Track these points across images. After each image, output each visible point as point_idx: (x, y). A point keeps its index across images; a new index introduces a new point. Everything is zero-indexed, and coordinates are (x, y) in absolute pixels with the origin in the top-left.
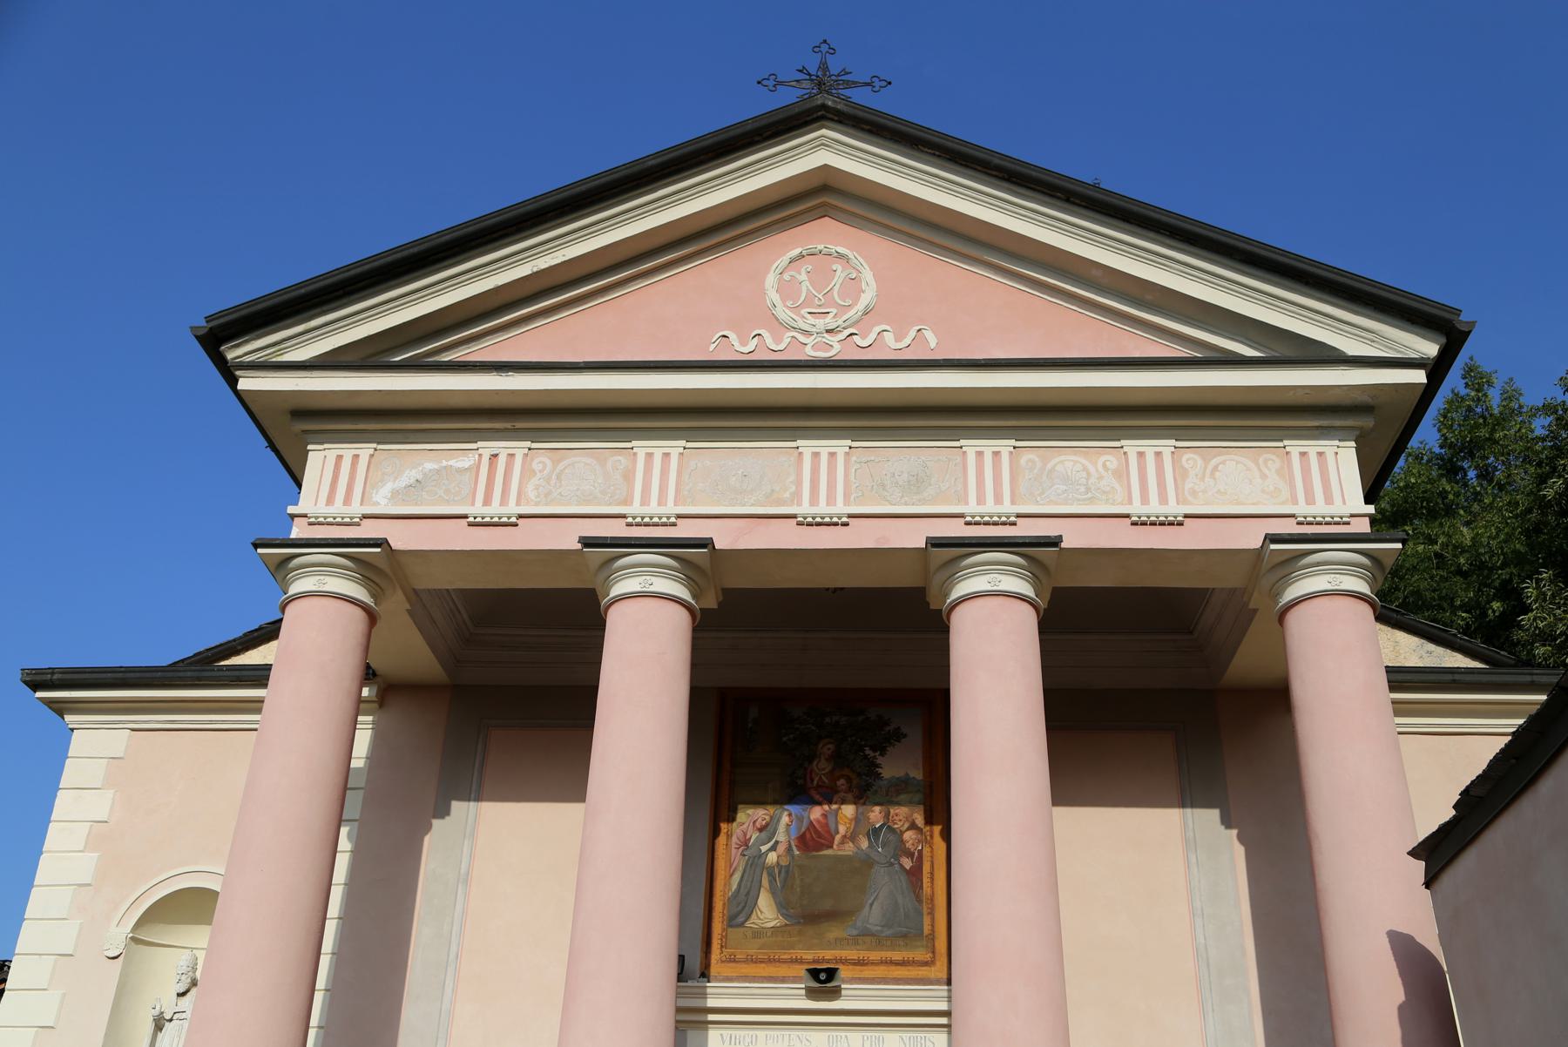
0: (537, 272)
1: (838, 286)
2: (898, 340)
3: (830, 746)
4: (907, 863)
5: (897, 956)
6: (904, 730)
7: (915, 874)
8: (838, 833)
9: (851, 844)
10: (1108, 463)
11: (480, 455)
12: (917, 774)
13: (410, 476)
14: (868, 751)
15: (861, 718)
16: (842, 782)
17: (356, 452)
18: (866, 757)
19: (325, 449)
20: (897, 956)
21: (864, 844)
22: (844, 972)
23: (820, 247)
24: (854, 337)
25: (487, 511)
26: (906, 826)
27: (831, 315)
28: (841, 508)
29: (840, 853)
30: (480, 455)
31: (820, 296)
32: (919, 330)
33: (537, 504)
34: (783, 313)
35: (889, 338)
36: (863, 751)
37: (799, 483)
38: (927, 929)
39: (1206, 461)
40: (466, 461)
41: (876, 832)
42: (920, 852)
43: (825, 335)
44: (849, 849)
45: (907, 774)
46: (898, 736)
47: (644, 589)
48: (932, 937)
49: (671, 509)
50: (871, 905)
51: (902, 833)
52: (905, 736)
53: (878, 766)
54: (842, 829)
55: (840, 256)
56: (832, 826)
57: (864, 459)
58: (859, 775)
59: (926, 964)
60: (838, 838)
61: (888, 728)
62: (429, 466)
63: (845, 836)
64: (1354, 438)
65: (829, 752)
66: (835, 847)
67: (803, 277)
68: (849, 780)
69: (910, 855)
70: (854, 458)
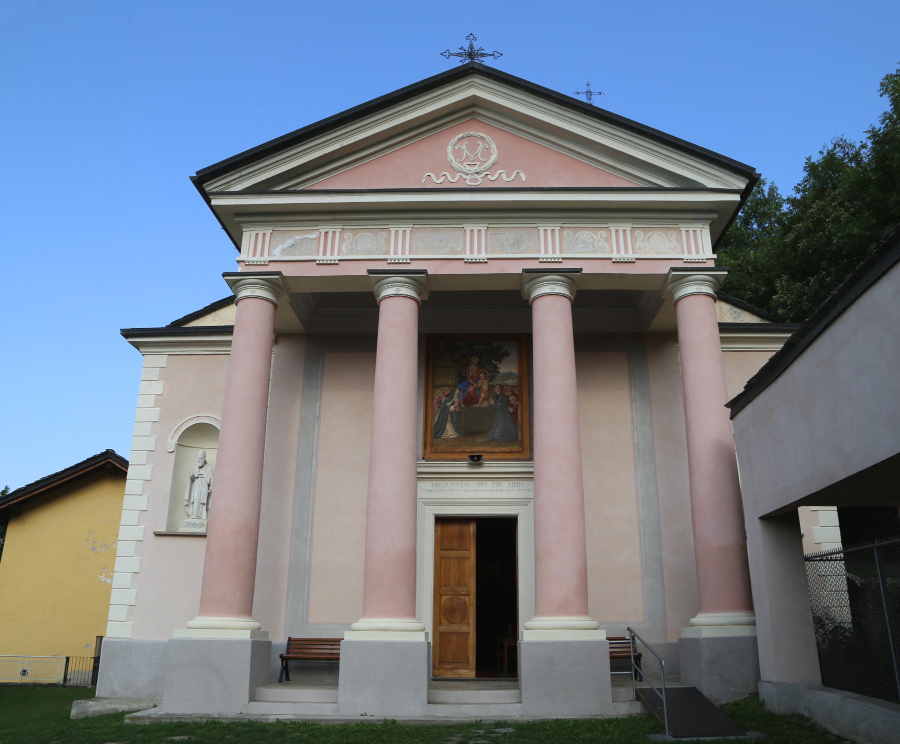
0: (343, 147)
1: (480, 153)
2: (508, 177)
3: (477, 359)
4: (511, 410)
5: (507, 449)
6: (509, 352)
7: (514, 415)
8: (480, 397)
9: (486, 402)
10: (602, 235)
11: (320, 232)
12: (515, 371)
13: (289, 242)
14: (493, 361)
16: (482, 375)
17: (264, 232)
18: (492, 364)
19: (250, 231)
20: (507, 449)
21: (492, 402)
22: (485, 456)
23: (472, 133)
24: (488, 176)
25: (325, 258)
26: (511, 394)
27: (477, 165)
28: (484, 255)
29: (482, 406)
30: (320, 232)
31: (472, 156)
32: (518, 173)
33: (347, 254)
34: (456, 164)
35: (504, 176)
36: (491, 361)
37: (465, 244)
38: (520, 438)
39: (354, 235)
40: (314, 236)
41: (498, 397)
42: (517, 405)
43: (475, 175)
44: (485, 404)
45: (511, 371)
46: (506, 354)
47: (397, 293)
48: (522, 441)
49: (408, 256)
50: (496, 427)
51: (509, 397)
52: (509, 354)
53: (498, 368)
54: (482, 396)
55: (481, 138)
56: (478, 394)
57: (494, 233)
58: (490, 372)
59: (519, 452)
60: (481, 399)
61: (502, 351)
62: (297, 237)
63: (483, 399)
64: (709, 224)
66: (479, 403)
67: (464, 147)
68: (485, 374)
69: (512, 406)
70: (489, 232)
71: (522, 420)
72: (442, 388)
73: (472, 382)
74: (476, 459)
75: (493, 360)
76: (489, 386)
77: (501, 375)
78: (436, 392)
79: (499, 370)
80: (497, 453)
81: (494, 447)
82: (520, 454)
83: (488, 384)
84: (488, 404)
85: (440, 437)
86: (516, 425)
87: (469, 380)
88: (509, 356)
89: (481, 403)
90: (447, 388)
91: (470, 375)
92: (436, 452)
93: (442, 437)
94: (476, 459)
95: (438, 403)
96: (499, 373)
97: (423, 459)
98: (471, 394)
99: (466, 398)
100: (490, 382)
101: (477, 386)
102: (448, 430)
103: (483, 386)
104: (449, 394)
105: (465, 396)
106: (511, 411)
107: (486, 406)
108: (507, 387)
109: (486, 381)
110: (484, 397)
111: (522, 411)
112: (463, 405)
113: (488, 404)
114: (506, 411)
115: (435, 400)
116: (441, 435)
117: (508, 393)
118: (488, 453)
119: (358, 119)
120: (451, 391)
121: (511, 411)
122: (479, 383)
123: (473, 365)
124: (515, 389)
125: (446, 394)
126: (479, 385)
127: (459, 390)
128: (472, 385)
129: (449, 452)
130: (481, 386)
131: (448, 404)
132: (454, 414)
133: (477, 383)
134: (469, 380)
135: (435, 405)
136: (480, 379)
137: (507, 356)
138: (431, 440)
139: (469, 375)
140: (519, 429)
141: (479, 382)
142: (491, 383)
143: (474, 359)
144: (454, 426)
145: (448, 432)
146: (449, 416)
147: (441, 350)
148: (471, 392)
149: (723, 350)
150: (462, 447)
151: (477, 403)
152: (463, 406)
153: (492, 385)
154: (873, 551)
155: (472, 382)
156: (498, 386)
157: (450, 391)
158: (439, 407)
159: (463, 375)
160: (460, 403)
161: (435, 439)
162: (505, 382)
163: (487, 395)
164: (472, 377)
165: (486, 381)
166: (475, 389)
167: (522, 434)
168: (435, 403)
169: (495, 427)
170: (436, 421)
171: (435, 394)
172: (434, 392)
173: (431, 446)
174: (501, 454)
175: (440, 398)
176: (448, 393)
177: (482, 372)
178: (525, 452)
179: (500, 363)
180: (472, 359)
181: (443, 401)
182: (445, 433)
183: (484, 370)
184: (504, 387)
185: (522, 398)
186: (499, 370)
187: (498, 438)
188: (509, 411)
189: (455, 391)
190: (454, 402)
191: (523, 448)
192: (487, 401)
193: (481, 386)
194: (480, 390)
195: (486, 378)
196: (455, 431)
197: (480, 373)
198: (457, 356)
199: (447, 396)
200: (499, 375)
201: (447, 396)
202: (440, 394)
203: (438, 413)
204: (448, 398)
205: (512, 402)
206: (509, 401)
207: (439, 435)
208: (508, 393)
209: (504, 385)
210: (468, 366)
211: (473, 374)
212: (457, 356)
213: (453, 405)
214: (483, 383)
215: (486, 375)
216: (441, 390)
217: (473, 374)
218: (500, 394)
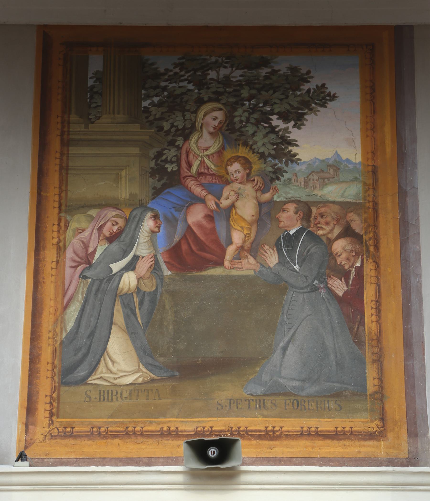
6: (331, 89)
8: (230, 242)
9: (251, 260)
14: (276, 121)
15: (264, 71)
18: (272, 130)
26: (337, 231)
29: (234, 272)
36: (268, 120)
42: (360, 270)
52: (333, 97)
53: (291, 143)
56: (222, 234)
58: (262, 156)
60: (231, 251)
61: (306, 87)
63: (241, 248)
65: (216, 123)
71: (379, 322)
72: (93, 212)
73: (198, 191)
74: (213, 453)
75: (275, 117)
76: (260, 204)
77: (304, 167)
78: (73, 225)
79: (294, 149)
80: (289, 436)
81: (280, 416)
82: (375, 443)
83: (257, 198)
84: (258, 268)
85: (83, 381)
86: (360, 343)
87: (191, 184)
88: (330, 104)
89: (231, 262)
90: (111, 213)
91: (194, 169)
92: (72, 435)
93: (92, 380)
94: (213, 453)
95: (80, 264)
96: (297, 162)
97: (22, 457)
98: (195, 229)
99: (178, 245)
100: (264, 192)
101: (217, 205)
102: (116, 357)
103: (238, 204)
104: (120, 232)
105: (177, 239)
106: (340, 293)
107: (251, 273)
108: (323, 210)
109: (248, 189)
110: (244, 242)
111: (378, 292)
112: (169, 269)
113: (258, 268)
114: (323, 292)
115: (69, 254)
116: (90, 374)
117: (328, 228)
118: (260, 437)
119: (242, 276)
120: (127, 221)
121: (340, 293)
122: (225, 194)
123: (205, 131)
124: (352, 216)
125: (106, 232)
126: (225, 203)
127: (156, 217)
128: (202, 201)
129: (115, 436)
130: (233, 206)
131: (116, 267)
132: (136, 300)
133: (219, 197)
134: (191, 184)
135: (68, 271)
136: (228, 183)
137: (324, 105)
138: (54, 389)
139: (190, 165)
140: (369, 356)
141: (226, 191)
142: (267, 196)
143: (214, 110)
144: (134, 342)
145: (113, 362)
146: (118, 307)
147: (90, 83)
148: (200, 226)
149: (110, 392)
150: (164, 416)
151: (220, 263)
152: (167, 272)
153: (271, 202)
154: (133, 296)
155: (198, 191)
156: (291, 207)
157: (121, 222)
158: (84, 277)
159: (170, 168)
160: (157, 262)
161: (64, 389)
162: (320, 193)
163: (253, 235)
164: (200, 174)
165: (248, 189)
166: (210, 218)
167: (381, 370)
168: (68, 263)
169: (282, 344)
170: (70, 325)
171: (69, 233)
172: (67, 227)
173: (52, 414)
174: (303, 442)
175: (86, 246)
176: (115, 228)
177: (237, 159)
178: (390, 435)
179: (297, 126)
180: (201, 114)
181: (97, 256)
182: (102, 367)
183: (242, 151)
184: (314, 210)
185: (377, 247)
186: (294, 149)
187: (296, 384)
188: (331, 291)
189: (140, 221)
190: (136, 258)
191: (383, 419)
192: (255, 258)
193: (233, 206)
194: (228, 218)
195: (249, 178)
196: (140, 359)
197: (231, 161)
198: (145, 104)
199: (111, 239)
200: (297, 168)
201: (111, 239)
202: (86, 234)
203: (80, 298)
204: (115, 246)
205: (341, 260)
206: (331, 256)
207: (81, 373)
208: (328, 228)
209: (316, 203)
210: (187, 138)
211: (202, 162)
212: (145, 104)
213: (133, 269)
214: (238, 195)
215: (251, 168)
216: (92, 218)
217: (202, 162)
218: (298, 233)
